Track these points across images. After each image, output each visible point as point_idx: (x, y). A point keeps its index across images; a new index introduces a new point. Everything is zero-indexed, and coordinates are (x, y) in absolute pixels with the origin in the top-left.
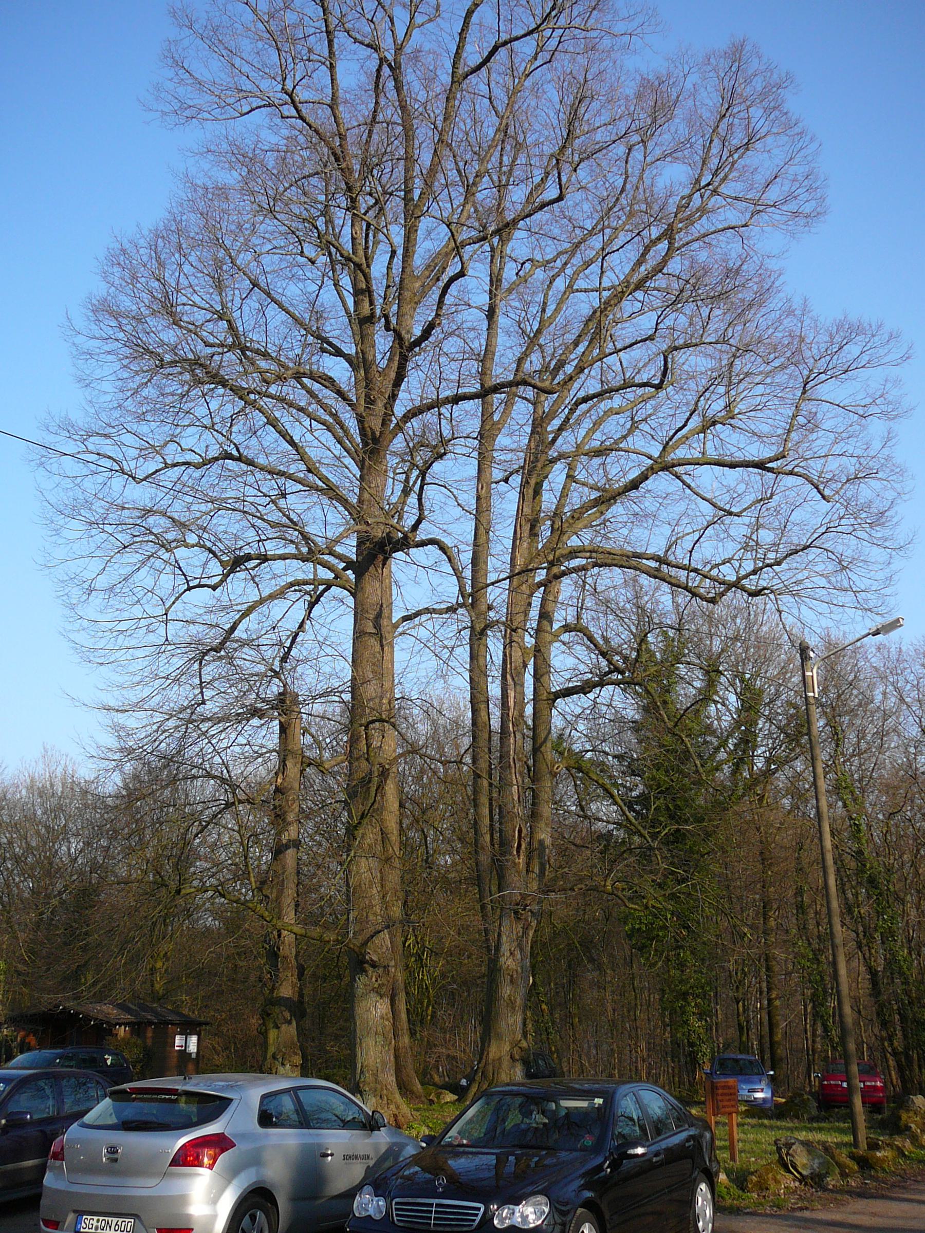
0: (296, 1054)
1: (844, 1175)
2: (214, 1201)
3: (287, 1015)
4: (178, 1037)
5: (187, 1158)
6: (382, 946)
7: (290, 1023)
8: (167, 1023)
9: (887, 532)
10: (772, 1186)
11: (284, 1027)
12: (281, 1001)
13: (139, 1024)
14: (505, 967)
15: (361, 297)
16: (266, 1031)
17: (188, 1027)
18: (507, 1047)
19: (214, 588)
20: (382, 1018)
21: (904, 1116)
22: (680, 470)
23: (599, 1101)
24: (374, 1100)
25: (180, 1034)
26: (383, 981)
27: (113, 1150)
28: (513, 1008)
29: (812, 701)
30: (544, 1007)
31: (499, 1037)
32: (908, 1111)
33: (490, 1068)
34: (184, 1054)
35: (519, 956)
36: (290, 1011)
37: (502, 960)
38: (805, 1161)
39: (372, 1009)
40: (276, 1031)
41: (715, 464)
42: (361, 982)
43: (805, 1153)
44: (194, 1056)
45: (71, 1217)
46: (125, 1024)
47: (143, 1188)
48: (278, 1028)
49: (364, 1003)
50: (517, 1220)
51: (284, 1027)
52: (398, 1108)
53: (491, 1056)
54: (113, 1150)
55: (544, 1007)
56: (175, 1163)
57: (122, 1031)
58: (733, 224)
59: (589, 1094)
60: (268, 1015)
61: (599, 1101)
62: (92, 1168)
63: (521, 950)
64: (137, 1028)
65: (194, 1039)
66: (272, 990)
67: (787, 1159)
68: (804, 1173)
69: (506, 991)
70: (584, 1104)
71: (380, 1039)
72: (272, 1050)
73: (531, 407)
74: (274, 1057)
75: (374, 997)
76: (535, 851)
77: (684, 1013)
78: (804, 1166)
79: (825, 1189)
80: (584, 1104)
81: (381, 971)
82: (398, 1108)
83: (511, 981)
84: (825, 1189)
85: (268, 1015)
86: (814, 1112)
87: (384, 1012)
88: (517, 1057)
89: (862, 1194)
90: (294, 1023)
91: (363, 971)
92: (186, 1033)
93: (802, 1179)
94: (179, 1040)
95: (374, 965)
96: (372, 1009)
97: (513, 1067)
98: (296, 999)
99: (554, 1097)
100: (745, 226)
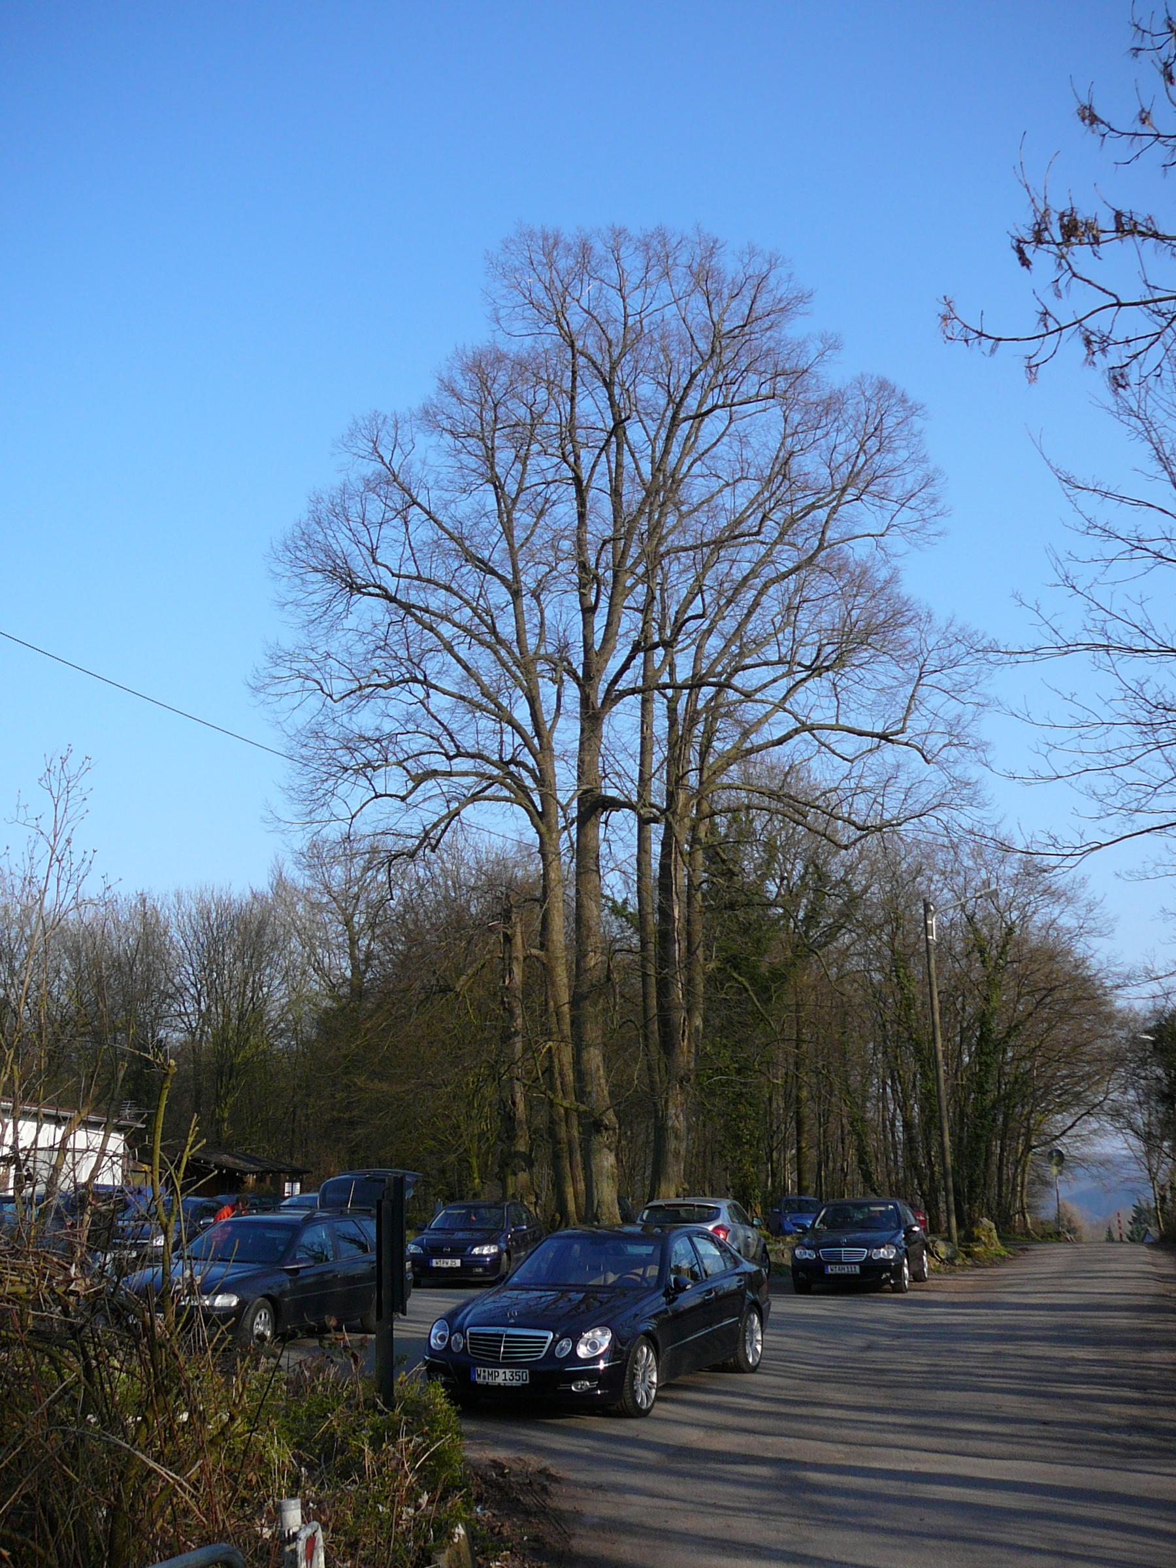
6: (610, 1118)
12: (517, 1154)
16: (505, 1178)
21: (976, 1231)
23: (891, 1207)
32: (978, 1227)
46: (253, 1173)
57: (251, 1179)
61: (891, 1207)
69: (672, 1144)
75: (605, 1150)
91: (599, 1132)
92: (293, 1182)
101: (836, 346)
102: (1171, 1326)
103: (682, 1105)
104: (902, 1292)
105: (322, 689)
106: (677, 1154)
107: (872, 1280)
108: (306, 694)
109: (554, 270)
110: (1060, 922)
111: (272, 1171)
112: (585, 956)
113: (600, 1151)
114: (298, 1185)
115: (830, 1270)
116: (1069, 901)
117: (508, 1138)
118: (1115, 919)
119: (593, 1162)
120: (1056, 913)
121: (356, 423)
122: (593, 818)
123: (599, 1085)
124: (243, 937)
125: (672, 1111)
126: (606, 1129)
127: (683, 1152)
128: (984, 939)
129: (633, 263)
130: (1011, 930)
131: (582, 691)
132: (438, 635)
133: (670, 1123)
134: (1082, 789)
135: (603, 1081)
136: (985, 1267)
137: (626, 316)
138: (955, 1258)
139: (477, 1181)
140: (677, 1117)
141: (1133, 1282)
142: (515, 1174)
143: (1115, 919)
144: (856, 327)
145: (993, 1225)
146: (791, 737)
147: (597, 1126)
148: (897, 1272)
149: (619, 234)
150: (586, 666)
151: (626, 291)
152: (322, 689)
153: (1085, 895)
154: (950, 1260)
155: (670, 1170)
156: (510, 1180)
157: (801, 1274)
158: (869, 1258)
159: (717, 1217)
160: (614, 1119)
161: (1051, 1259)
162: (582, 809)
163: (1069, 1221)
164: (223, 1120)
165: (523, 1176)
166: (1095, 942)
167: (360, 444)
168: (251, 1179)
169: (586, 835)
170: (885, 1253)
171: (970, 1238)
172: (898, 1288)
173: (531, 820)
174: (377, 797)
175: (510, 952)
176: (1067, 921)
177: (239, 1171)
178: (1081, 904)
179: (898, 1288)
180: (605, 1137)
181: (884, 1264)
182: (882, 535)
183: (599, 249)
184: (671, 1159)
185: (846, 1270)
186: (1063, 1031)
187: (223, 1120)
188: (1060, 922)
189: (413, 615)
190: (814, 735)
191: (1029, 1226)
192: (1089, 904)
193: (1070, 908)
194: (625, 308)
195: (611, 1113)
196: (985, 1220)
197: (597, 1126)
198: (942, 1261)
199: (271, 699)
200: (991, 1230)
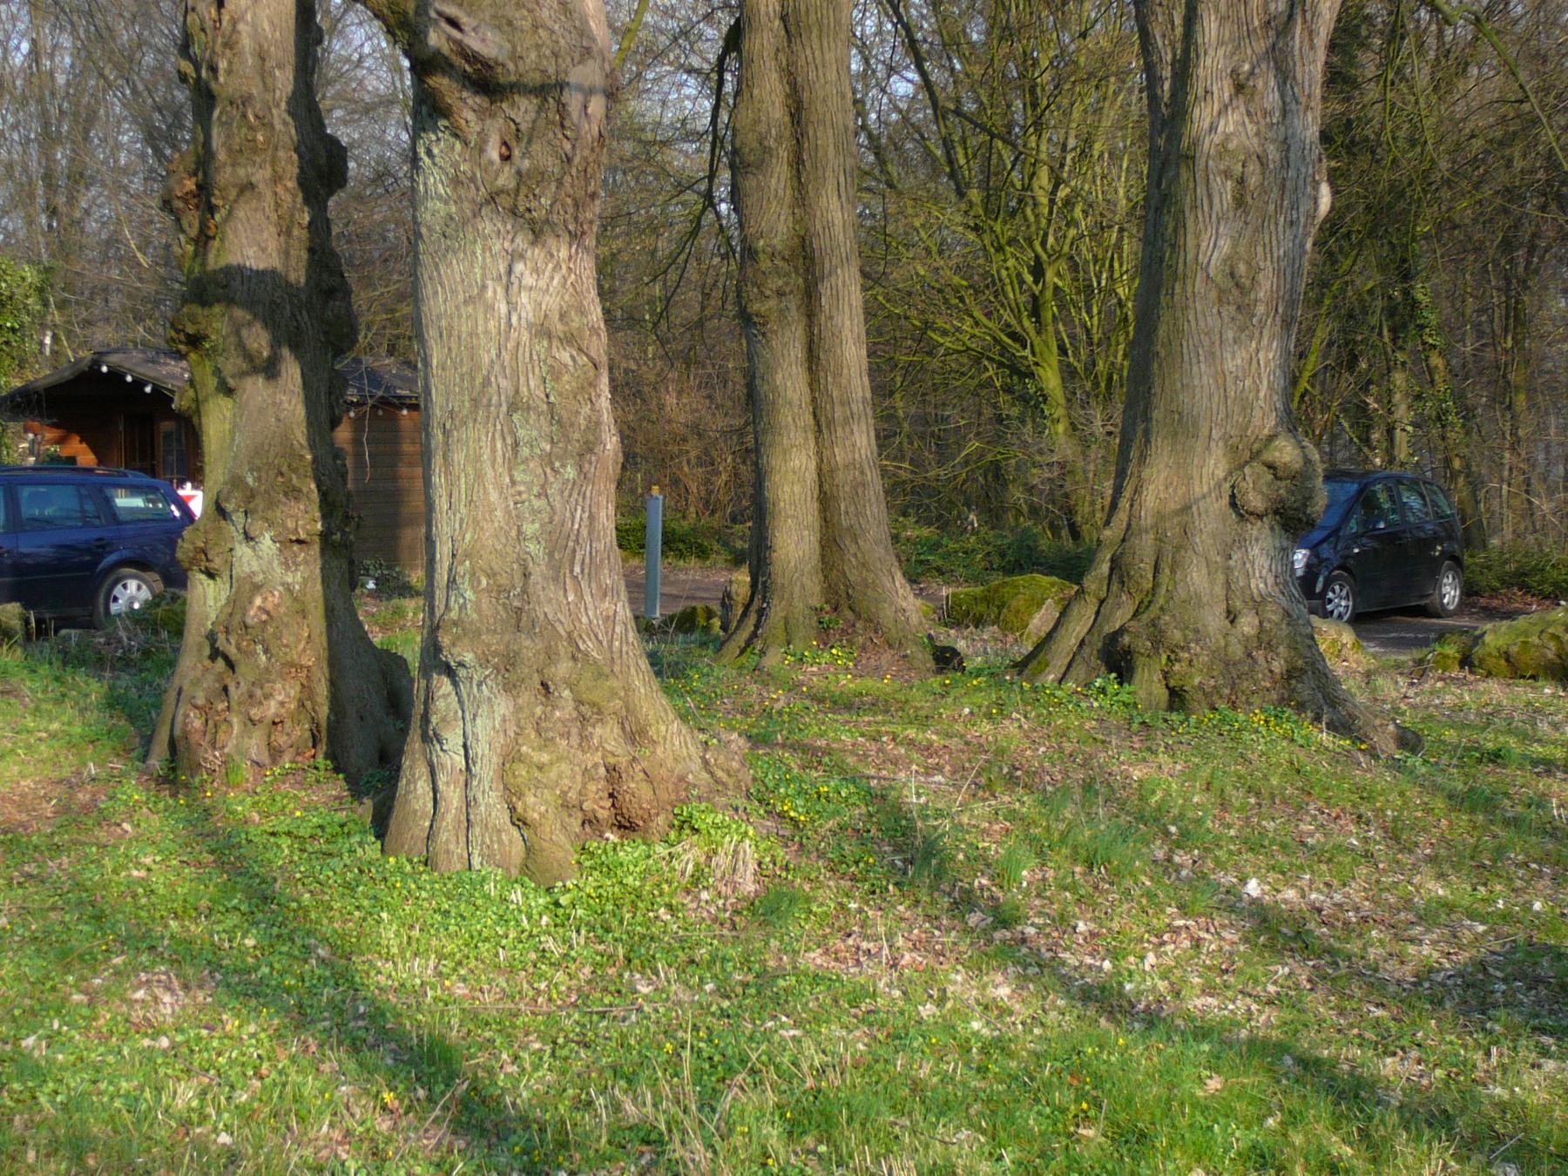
0: (294, 493)
3: (259, 340)
7: (270, 370)
11: (255, 389)
14: (1208, 144)
18: (1214, 466)
20: (542, 331)
24: (503, 706)
26: (542, 156)
28: (1245, 309)
30: (1436, 360)
31: (1184, 428)
33: (1145, 545)
35: (1272, 99)
36: (271, 323)
37: (1201, 116)
39: (495, 292)
48: (229, 392)
52: (636, 735)
53: (1151, 498)
55: (1436, 360)
63: (1285, 76)
66: (203, 240)
71: (530, 430)
75: (494, 238)
81: (523, 109)
82: (636, 735)
83: (1239, 202)
87: (552, 302)
88: (1256, 501)
90: (292, 371)
96: (495, 292)
97: (1241, 542)
98: (298, 275)
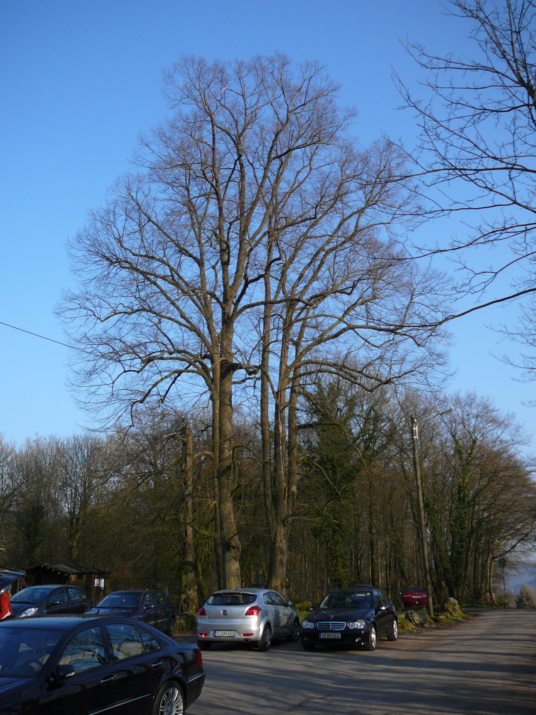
1: (430, 624)
2: (259, 626)
3: (191, 568)
4: (96, 580)
5: (250, 613)
6: (236, 541)
7: (192, 572)
8: (92, 573)
9: (446, 368)
10: (407, 628)
12: (187, 563)
13: (80, 574)
15: (223, 253)
16: (181, 576)
17: (100, 575)
19: (138, 372)
21: (446, 605)
22: (356, 330)
23: (369, 594)
25: (97, 578)
27: (225, 611)
29: (415, 440)
32: (447, 603)
34: (98, 587)
38: (417, 618)
40: (186, 576)
41: (372, 328)
42: (228, 555)
43: (417, 616)
44: (103, 589)
45: (212, 632)
46: (75, 574)
47: (237, 622)
48: (186, 574)
49: (229, 563)
50: (356, 626)
51: (189, 574)
54: (225, 611)
56: (246, 614)
57: (73, 577)
58: (384, 222)
59: (365, 592)
60: (182, 569)
61: (369, 594)
62: (218, 617)
64: (79, 576)
65: (103, 581)
67: (411, 618)
68: (417, 623)
69: (279, 557)
70: (364, 595)
71: (236, 578)
72: (184, 584)
73: (278, 282)
74: (185, 586)
75: (234, 561)
76: (291, 494)
77: (337, 566)
78: (417, 620)
79: (425, 628)
80: (364, 595)
81: (236, 550)
84: (425, 628)
85: (182, 569)
86: (403, 608)
89: (438, 629)
91: (229, 550)
92: (99, 578)
93: (416, 625)
94: (96, 581)
95: (234, 548)
99: (354, 593)
100: (389, 223)
101: (354, 115)
102: (533, 689)
103: (284, 535)
104: (370, 650)
105: (94, 315)
106: (281, 562)
107: (349, 643)
108: (88, 317)
109: (204, 82)
110: (502, 437)
111: (86, 573)
112: (224, 451)
113: (230, 560)
114: (103, 580)
115: (323, 636)
116: (506, 426)
117: (183, 553)
118: (532, 435)
119: (227, 567)
120: (499, 433)
121: (119, 179)
122: (228, 376)
123: (230, 523)
124: (95, 457)
125: (278, 539)
126: (234, 548)
127: (285, 561)
128: (461, 446)
129: (250, 82)
130: (474, 442)
131: (223, 309)
132: (158, 286)
133: (277, 545)
134: (501, 358)
135: (233, 521)
136: (443, 629)
137: (246, 109)
138: (425, 623)
139: (201, 577)
140: (281, 541)
141: (521, 644)
142: (186, 574)
143: (532, 435)
144: (373, 116)
145: (456, 602)
146: (342, 333)
147: (227, 547)
148: (366, 636)
149: (241, 65)
150: (225, 294)
151: (246, 97)
152: (94, 315)
153: (514, 422)
154: (422, 625)
155: (277, 571)
156: (184, 578)
157: (305, 638)
158: (347, 628)
159: (254, 601)
160: (238, 542)
161: (488, 621)
162: (222, 371)
163: (527, 594)
164: (73, 547)
165: (191, 575)
166: (520, 447)
167: (122, 191)
168: (73, 577)
169: (224, 385)
170: (359, 625)
171: (443, 610)
172: (368, 647)
173: (206, 382)
174: (125, 372)
175: (186, 451)
176: (506, 436)
177: (66, 573)
178: (512, 428)
179: (368, 647)
180: (232, 553)
181: (357, 632)
182: (389, 223)
183: (230, 71)
184: (278, 565)
185: (332, 636)
186: (506, 496)
187: (73, 547)
188: (502, 437)
189: (149, 279)
190: (355, 332)
191: (494, 599)
192: (517, 428)
193: (507, 430)
194: (245, 105)
195: (237, 537)
196: (452, 599)
197: (227, 547)
198: (416, 625)
199: (68, 320)
200: (455, 604)
